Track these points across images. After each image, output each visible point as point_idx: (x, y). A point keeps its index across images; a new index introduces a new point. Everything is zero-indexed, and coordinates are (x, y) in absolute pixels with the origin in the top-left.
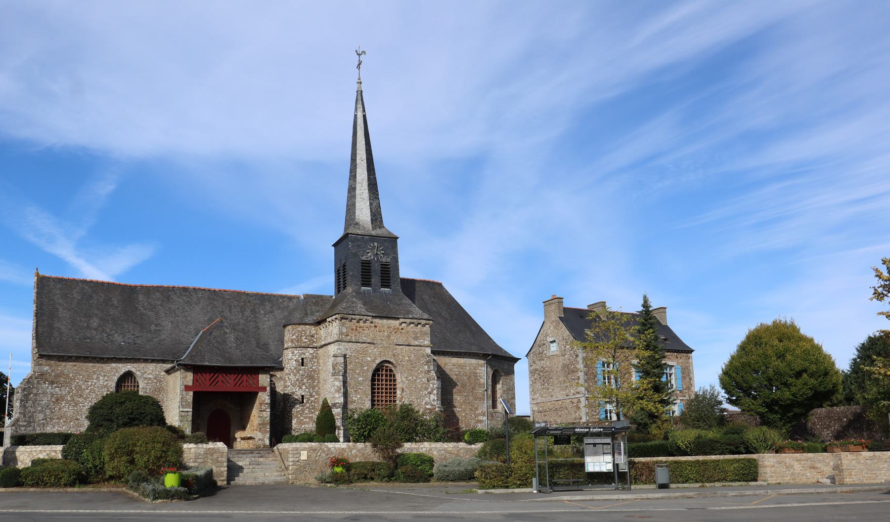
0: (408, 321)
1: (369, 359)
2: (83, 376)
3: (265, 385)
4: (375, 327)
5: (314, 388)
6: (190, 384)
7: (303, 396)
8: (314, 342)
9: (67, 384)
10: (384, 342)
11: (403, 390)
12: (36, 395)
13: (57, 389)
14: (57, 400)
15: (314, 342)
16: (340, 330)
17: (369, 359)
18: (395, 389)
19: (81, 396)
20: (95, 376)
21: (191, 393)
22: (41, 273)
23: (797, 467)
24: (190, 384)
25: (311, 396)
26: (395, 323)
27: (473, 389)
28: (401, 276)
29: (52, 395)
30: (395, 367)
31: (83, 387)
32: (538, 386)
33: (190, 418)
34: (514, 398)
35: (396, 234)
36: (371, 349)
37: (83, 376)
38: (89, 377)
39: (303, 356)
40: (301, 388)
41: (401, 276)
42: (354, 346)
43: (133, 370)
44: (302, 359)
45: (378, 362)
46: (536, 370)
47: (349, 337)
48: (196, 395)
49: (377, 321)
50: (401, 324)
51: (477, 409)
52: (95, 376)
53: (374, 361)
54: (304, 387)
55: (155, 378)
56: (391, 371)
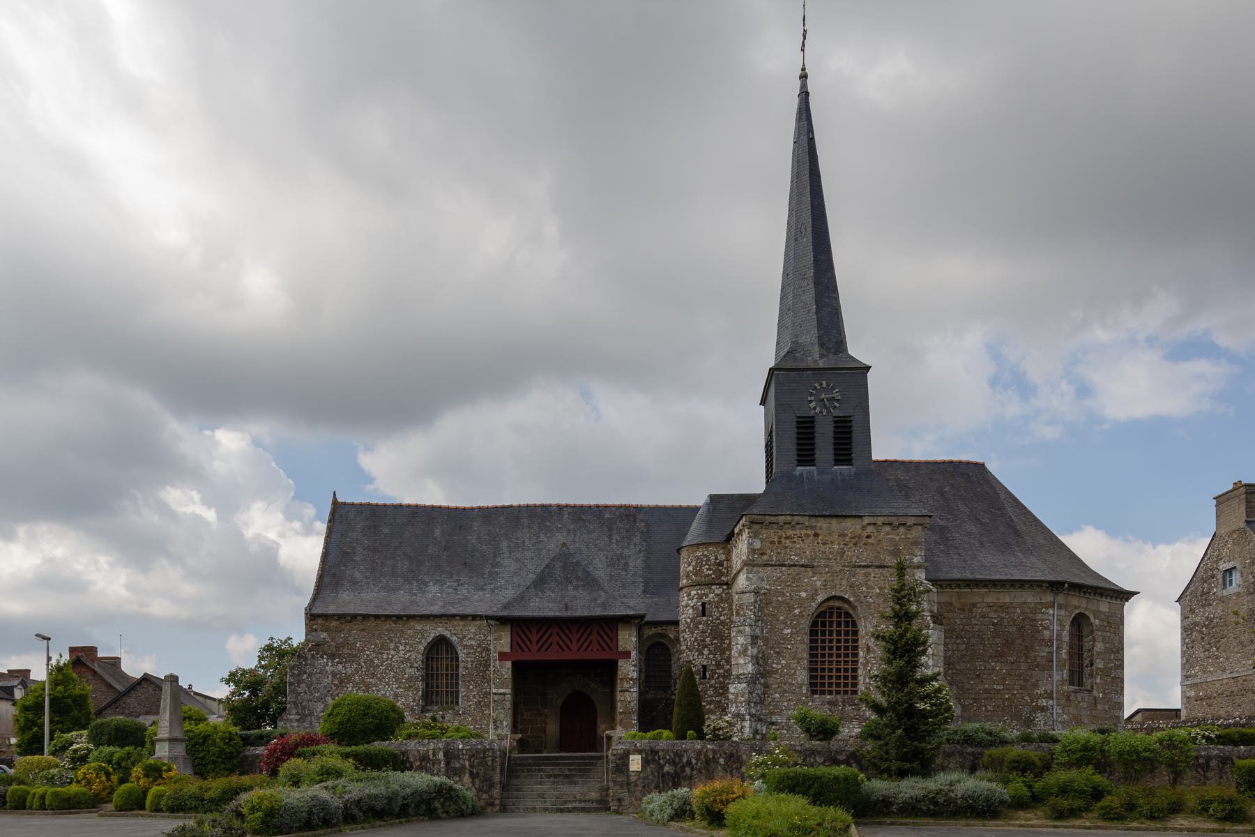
0: (880, 521)
1: (803, 594)
2: (376, 645)
3: (628, 648)
4: (816, 535)
5: (723, 652)
6: (507, 649)
7: (704, 667)
8: (722, 574)
9: (353, 658)
10: (832, 563)
11: (868, 648)
12: (310, 675)
13: (340, 667)
14: (341, 682)
15: (722, 574)
16: (750, 544)
17: (803, 594)
18: (856, 648)
19: (374, 675)
20: (392, 646)
21: (509, 664)
22: (340, 500)
23: (628, 697)
24: (507, 649)
25: (718, 666)
26: (851, 526)
27: (1029, 648)
28: (874, 458)
29: (334, 674)
30: (854, 608)
31: (376, 662)
32: (1199, 653)
33: (508, 705)
34: (1121, 667)
35: (866, 362)
36: (807, 577)
37: (376, 645)
38: (385, 647)
39: (705, 599)
40: (701, 653)
41: (874, 458)
42: (776, 573)
43: (447, 634)
44: (703, 604)
45: (820, 599)
46: (1196, 624)
47: (765, 558)
48: (517, 667)
49: (822, 524)
50: (864, 528)
51: (1036, 685)
52: (392, 646)
53: (812, 597)
54: (706, 652)
55: (479, 646)
56: (848, 615)
